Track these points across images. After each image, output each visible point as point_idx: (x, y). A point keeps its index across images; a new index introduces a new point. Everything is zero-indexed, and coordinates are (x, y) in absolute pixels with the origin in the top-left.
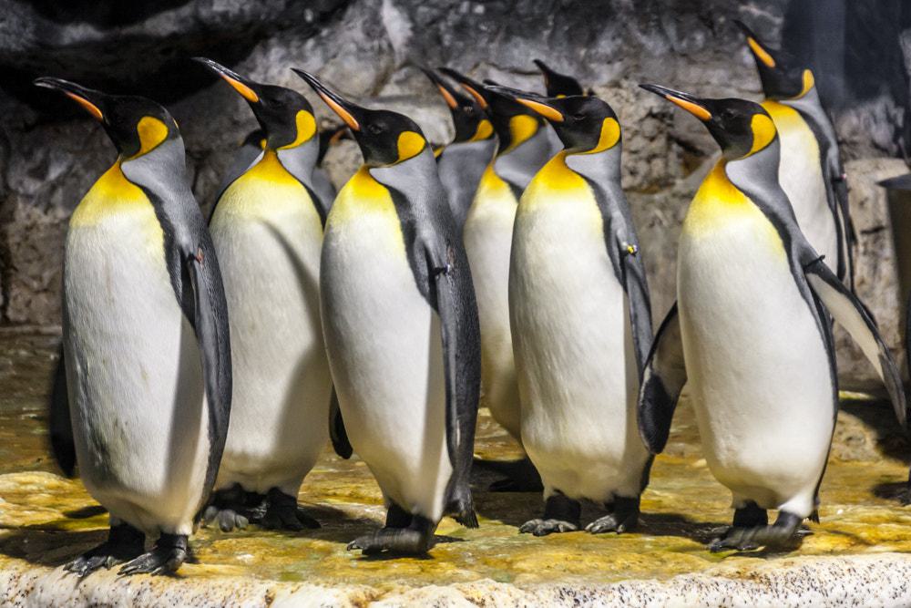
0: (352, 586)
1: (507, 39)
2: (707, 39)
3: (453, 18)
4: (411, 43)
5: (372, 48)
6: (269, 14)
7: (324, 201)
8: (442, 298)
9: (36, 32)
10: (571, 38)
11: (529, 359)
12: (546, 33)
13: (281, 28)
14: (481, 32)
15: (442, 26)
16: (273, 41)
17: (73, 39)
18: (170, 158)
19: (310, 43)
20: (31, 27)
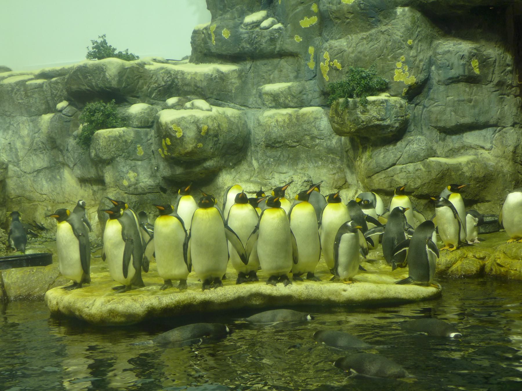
0: (445, 169)
1: (278, 166)
2: (322, 163)
3: (266, 162)
4: (258, 168)
5: (250, 170)
6: (220, 164)
7: (229, 233)
8: (460, 42)
9: (171, 172)
10: (293, 165)
11: (427, 61)
12: (287, 164)
13: (224, 167)
14: (272, 165)
15: (264, 164)
16: (223, 170)
17: (470, 87)
18: (280, 169)
19: (233, 170)
20: (170, 171)
